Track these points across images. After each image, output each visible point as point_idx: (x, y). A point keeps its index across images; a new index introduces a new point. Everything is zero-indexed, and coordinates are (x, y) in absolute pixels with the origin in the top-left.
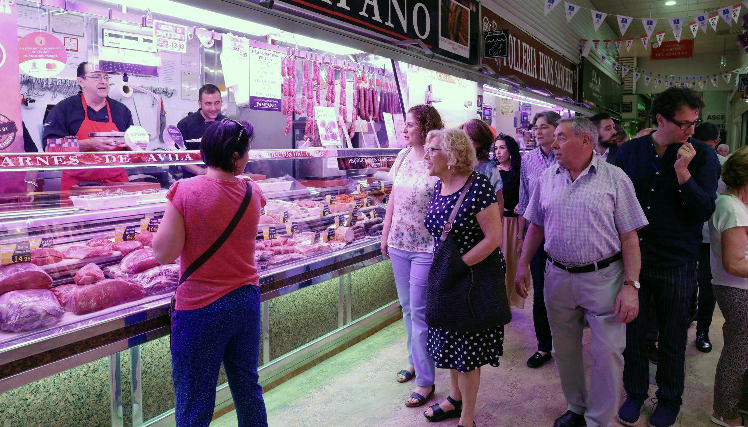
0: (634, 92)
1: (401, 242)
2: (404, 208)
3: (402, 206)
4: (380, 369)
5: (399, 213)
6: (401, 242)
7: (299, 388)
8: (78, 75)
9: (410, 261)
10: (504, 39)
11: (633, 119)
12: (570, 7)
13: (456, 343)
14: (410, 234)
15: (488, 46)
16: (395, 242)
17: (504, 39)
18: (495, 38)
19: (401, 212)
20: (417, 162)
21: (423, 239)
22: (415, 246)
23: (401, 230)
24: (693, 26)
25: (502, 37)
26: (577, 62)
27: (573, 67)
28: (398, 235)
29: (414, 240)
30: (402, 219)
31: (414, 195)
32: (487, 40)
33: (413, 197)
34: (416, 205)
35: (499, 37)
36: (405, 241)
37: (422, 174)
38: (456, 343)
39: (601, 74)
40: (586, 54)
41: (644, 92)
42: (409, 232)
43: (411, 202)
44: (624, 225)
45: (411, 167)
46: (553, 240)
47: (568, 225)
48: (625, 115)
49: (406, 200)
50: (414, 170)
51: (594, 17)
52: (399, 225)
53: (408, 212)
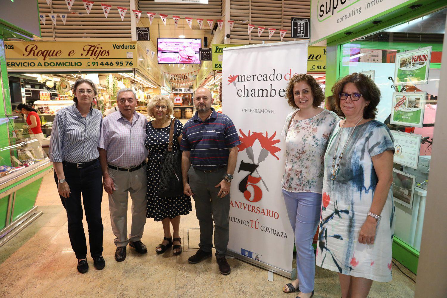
1: (290, 185)
2: (295, 158)
3: (293, 157)
4: (55, 253)
5: (291, 163)
6: (290, 185)
7: (18, 276)
8: (207, 38)
9: (298, 201)
10: (147, 32)
12: (52, 16)
14: (299, 178)
16: (286, 186)
17: (147, 32)
19: (292, 161)
20: (302, 120)
21: (308, 181)
22: (301, 187)
23: (292, 176)
24: (271, 31)
25: (146, 31)
28: (288, 180)
29: (300, 183)
30: (293, 166)
31: (303, 146)
32: (201, 52)
33: (303, 148)
34: (304, 154)
35: (145, 31)
36: (293, 184)
37: (307, 129)
42: (297, 177)
43: (300, 153)
44: (126, 142)
45: (298, 126)
46: (125, 154)
47: (133, 147)
49: (297, 151)
50: (301, 127)
51: (188, 22)
52: (290, 172)
53: (298, 161)
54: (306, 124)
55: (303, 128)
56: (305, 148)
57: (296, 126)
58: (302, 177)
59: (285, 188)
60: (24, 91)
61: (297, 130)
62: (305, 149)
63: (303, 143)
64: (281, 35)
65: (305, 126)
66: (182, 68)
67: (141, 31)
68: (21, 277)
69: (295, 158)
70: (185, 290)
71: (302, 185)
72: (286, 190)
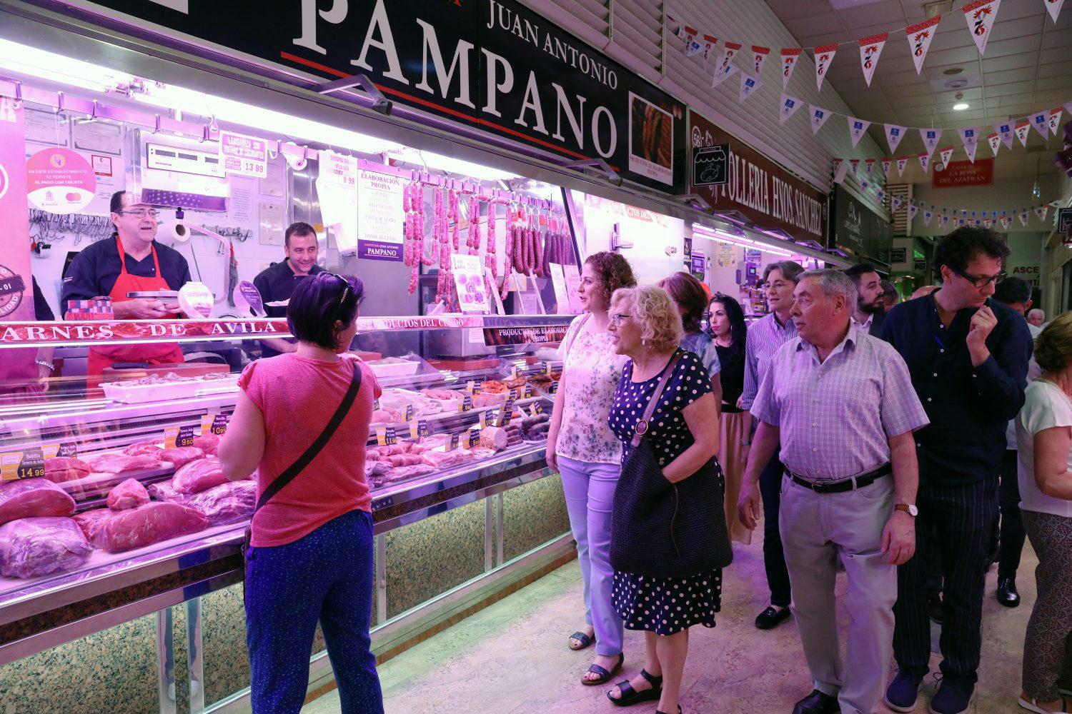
0: (908, 234)
1: (575, 449)
6: (575, 449)
9: (588, 476)
10: (723, 157)
11: (908, 273)
13: (653, 594)
15: (700, 168)
16: (565, 449)
17: (723, 157)
18: (710, 156)
21: (606, 444)
22: (595, 454)
25: (720, 154)
26: (828, 191)
27: (821, 197)
28: (570, 438)
31: (593, 381)
35: (716, 155)
36: (580, 448)
38: (653, 594)
39: (861, 208)
40: (839, 179)
41: (923, 234)
42: (586, 435)
43: (589, 392)
45: (588, 342)
48: (896, 267)
52: (572, 425)
54: (603, 341)
55: (597, 348)
56: (597, 384)
57: (585, 341)
58: (595, 436)
59: (564, 452)
60: (467, 304)
61: (587, 350)
62: (595, 387)
63: (593, 376)
64: (943, 159)
65: (601, 345)
66: (922, 256)
67: (703, 157)
68: (480, 650)
69: (579, 400)
70: (702, 689)
71: (596, 450)
72: (567, 456)
